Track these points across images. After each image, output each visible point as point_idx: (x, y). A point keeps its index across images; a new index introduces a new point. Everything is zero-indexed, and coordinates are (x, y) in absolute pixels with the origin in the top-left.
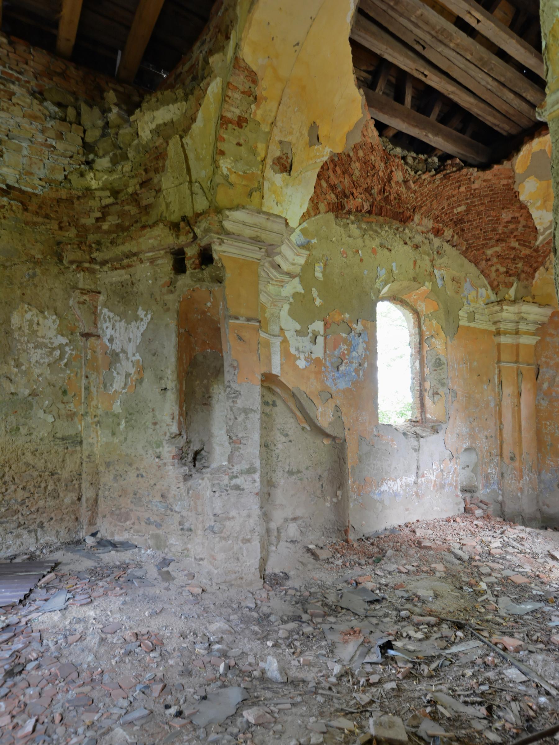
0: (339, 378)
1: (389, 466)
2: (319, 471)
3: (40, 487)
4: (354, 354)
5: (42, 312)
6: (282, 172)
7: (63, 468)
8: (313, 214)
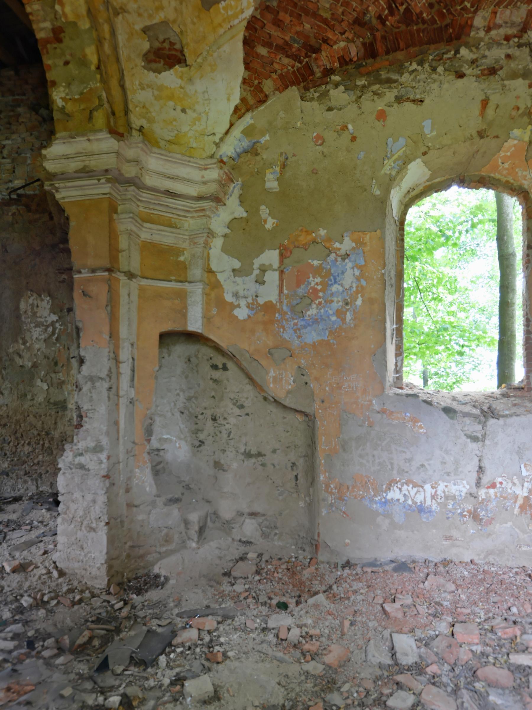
0: (305, 327)
1: (409, 460)
2: (292, 456)
3: (39, 444)
4: (335, 288)
5: (40, 296)
6: (171, 66)
7: (55, 429)
8: (251, 101)
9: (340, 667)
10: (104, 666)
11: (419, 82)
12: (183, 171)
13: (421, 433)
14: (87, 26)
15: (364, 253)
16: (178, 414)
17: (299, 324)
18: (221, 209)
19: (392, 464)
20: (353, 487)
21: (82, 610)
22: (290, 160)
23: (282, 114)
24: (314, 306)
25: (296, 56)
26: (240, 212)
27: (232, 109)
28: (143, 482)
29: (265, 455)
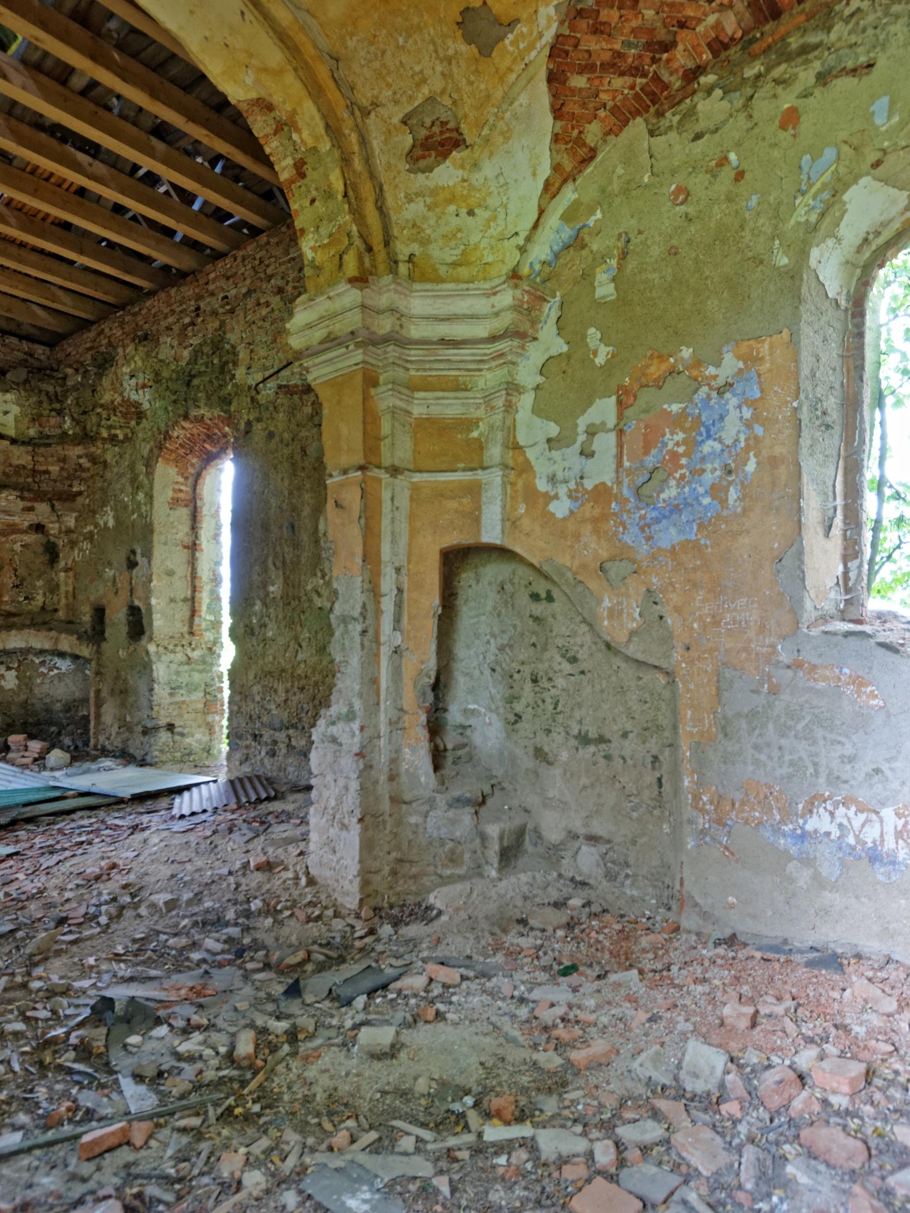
0: (658, 521)
6: (445, 155)
9: (588, 1069)
10: (294, 991)
11: (864, 30)
12: (461, 306)
13: (872, 707)
14: (328, 146)
15: (759, 376)
16: (488, 672)
17: (649, 516)
18: (531, 347)
19: (815, 764)
20: (743, 803)
21: (314, 930)
22: (634, 241)
23: (620, 170)
24: (673, 483)
25: (637, 69)
26: (560, 346)
27: (540, 186)
28: (416, 768)
29: (610, 741)
